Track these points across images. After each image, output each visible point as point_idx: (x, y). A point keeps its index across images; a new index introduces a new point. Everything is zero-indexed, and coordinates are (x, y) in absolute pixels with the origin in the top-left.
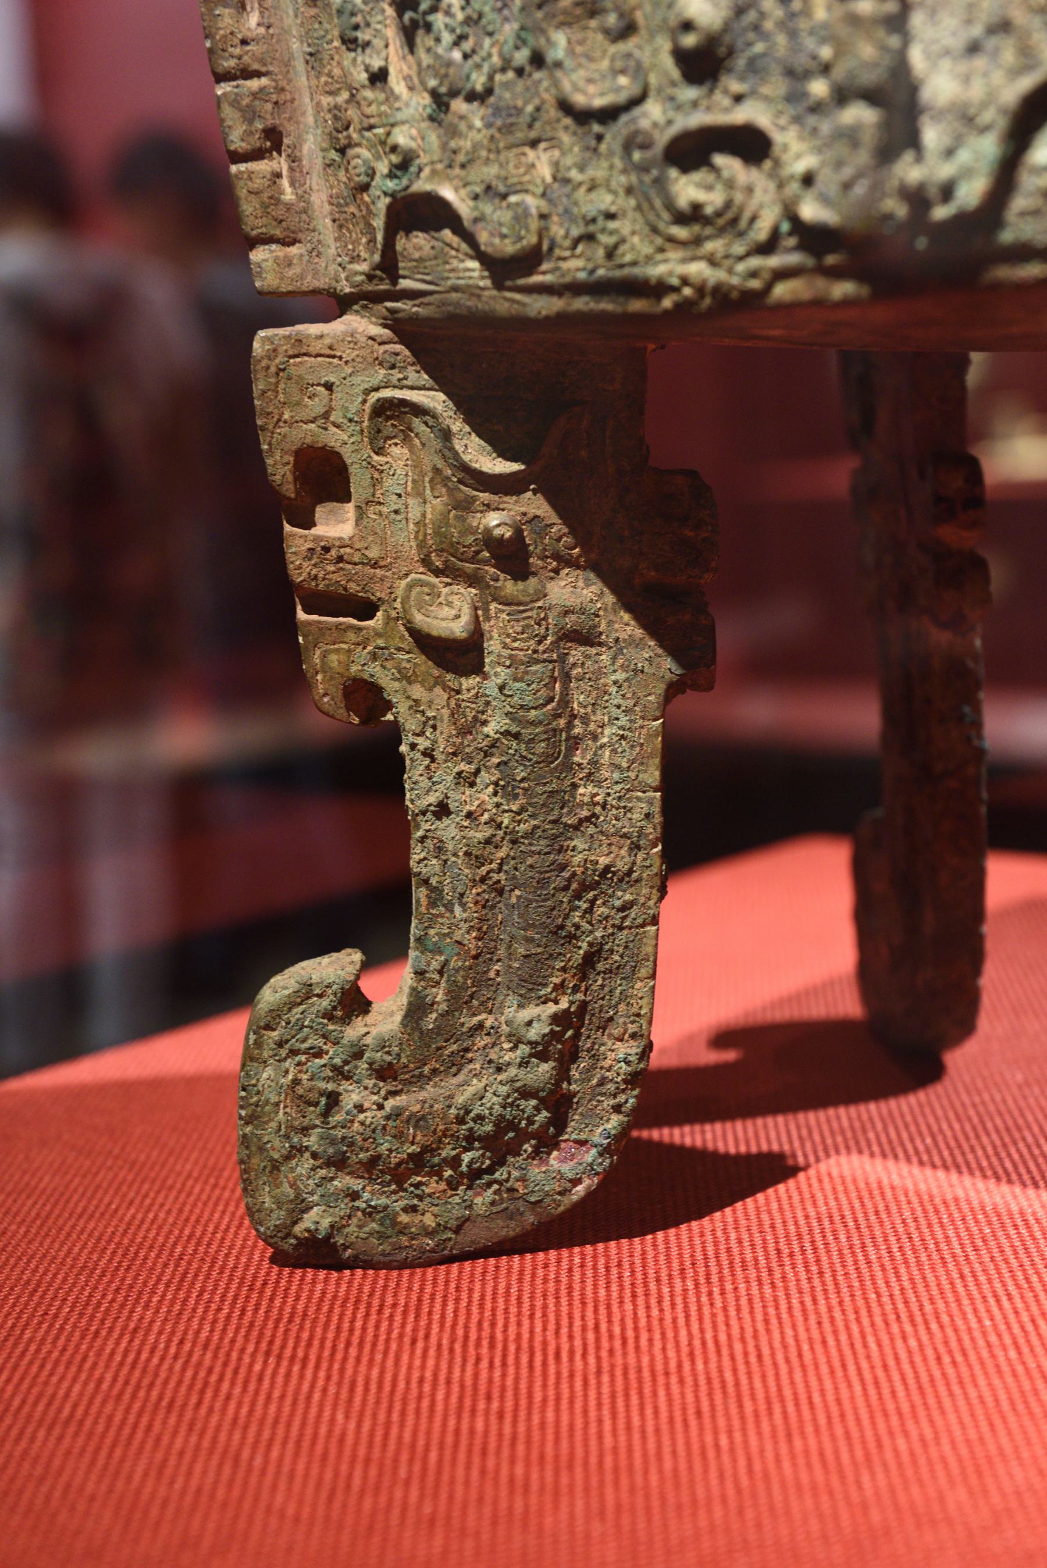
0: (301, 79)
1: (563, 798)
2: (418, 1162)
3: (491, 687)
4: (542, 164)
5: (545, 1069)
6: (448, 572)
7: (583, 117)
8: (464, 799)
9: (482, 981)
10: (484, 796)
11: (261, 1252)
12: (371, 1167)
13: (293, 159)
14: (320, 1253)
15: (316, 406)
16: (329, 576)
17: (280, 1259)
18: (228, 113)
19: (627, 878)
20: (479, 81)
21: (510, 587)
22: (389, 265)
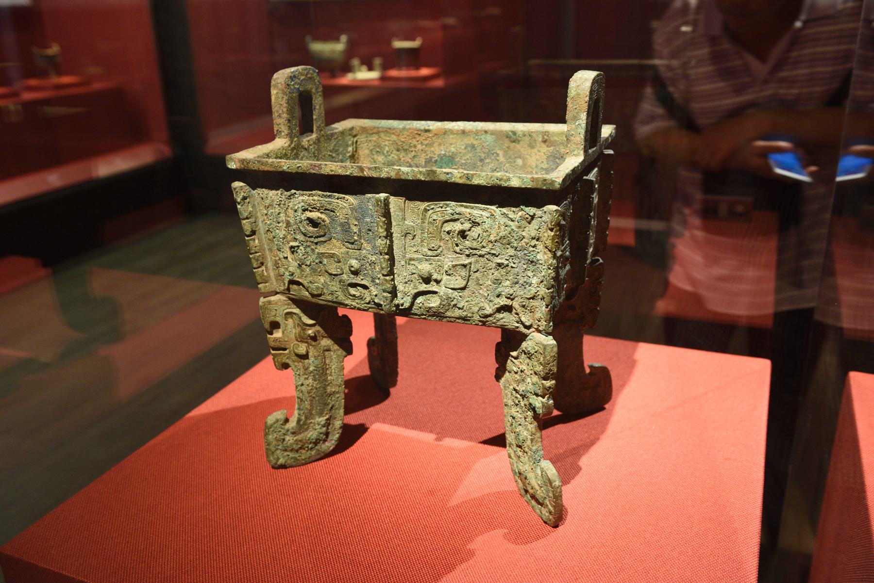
0: (267, 252)
1: (326, 380)
2: (301, 448)
3: (311, 361)
4: (322, 279)
5: (324, 429)
6: (302, 341)
7: (331, 274)
8: (307, 382)
9: (311, 414)
10: (310, 381)
11: (269, 467)
12: (292, 450)
13: (266, 267)
14: (283, 467)
15: (273, 314)
16: (277, 344)
17: (273, 467)
18: (253, 261)
19: (338, 393)
20: (308, 263)
21: (314, 343)
22: (288, 289)
